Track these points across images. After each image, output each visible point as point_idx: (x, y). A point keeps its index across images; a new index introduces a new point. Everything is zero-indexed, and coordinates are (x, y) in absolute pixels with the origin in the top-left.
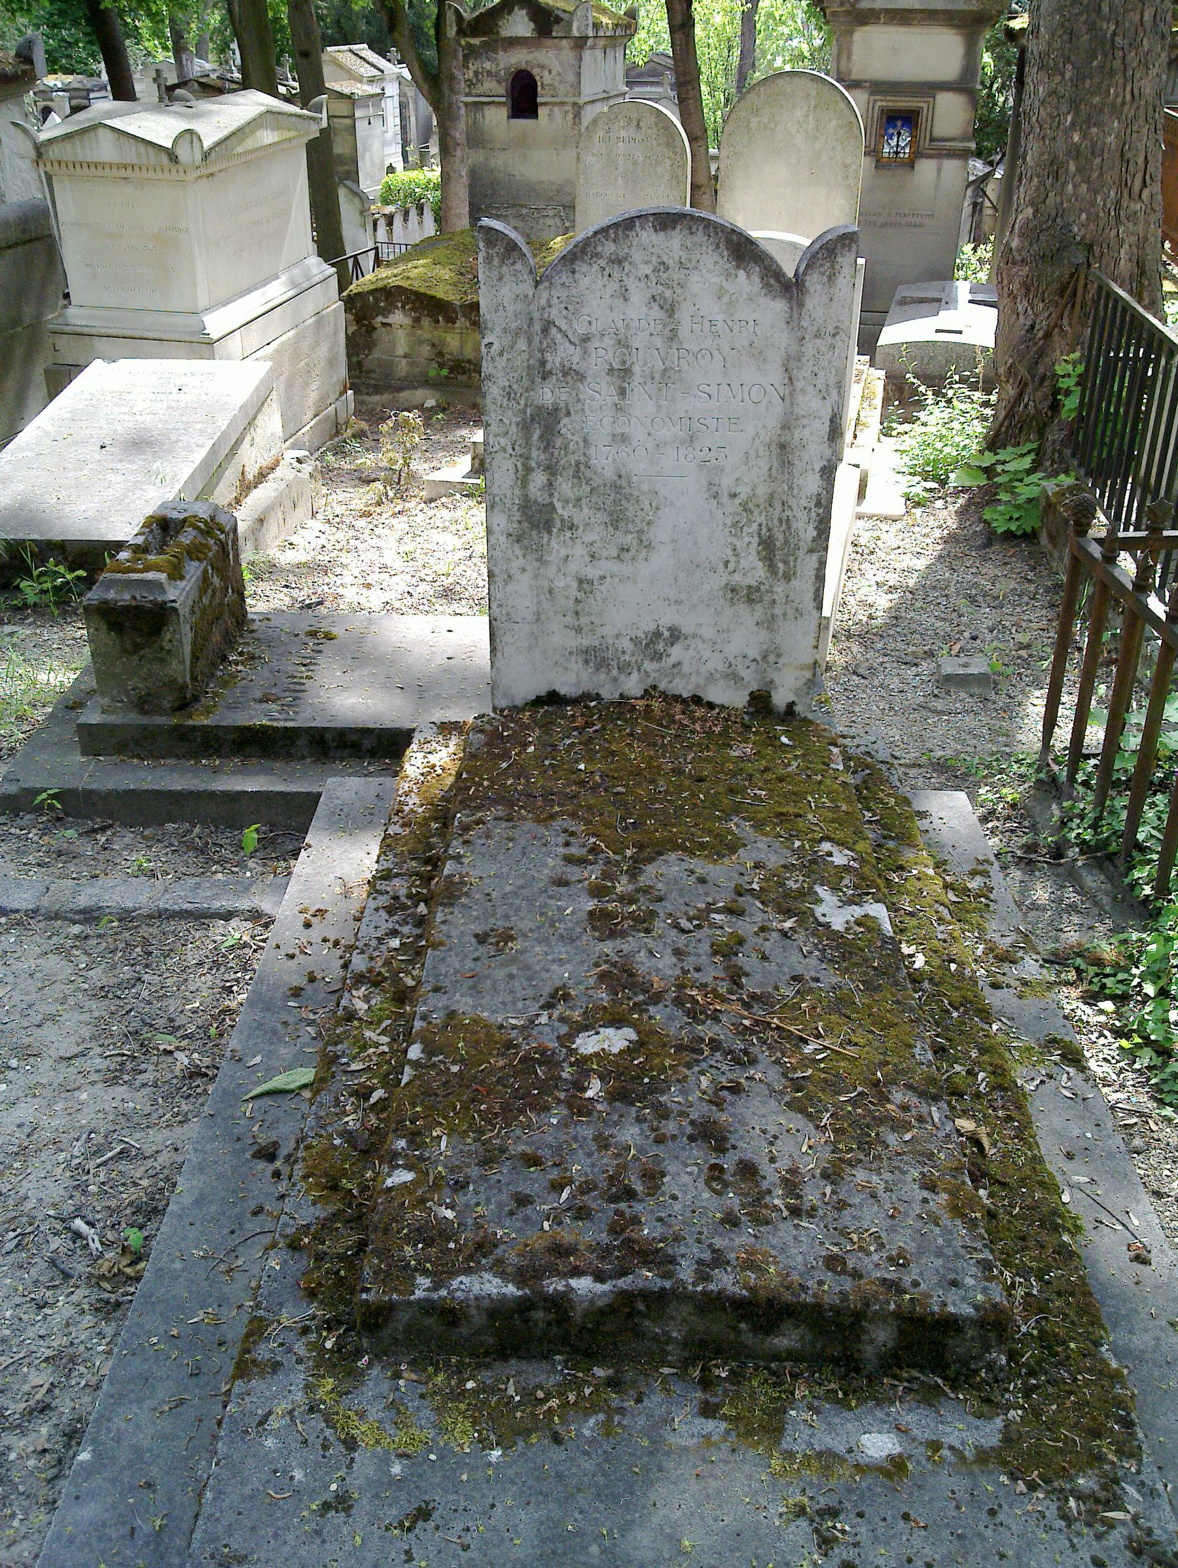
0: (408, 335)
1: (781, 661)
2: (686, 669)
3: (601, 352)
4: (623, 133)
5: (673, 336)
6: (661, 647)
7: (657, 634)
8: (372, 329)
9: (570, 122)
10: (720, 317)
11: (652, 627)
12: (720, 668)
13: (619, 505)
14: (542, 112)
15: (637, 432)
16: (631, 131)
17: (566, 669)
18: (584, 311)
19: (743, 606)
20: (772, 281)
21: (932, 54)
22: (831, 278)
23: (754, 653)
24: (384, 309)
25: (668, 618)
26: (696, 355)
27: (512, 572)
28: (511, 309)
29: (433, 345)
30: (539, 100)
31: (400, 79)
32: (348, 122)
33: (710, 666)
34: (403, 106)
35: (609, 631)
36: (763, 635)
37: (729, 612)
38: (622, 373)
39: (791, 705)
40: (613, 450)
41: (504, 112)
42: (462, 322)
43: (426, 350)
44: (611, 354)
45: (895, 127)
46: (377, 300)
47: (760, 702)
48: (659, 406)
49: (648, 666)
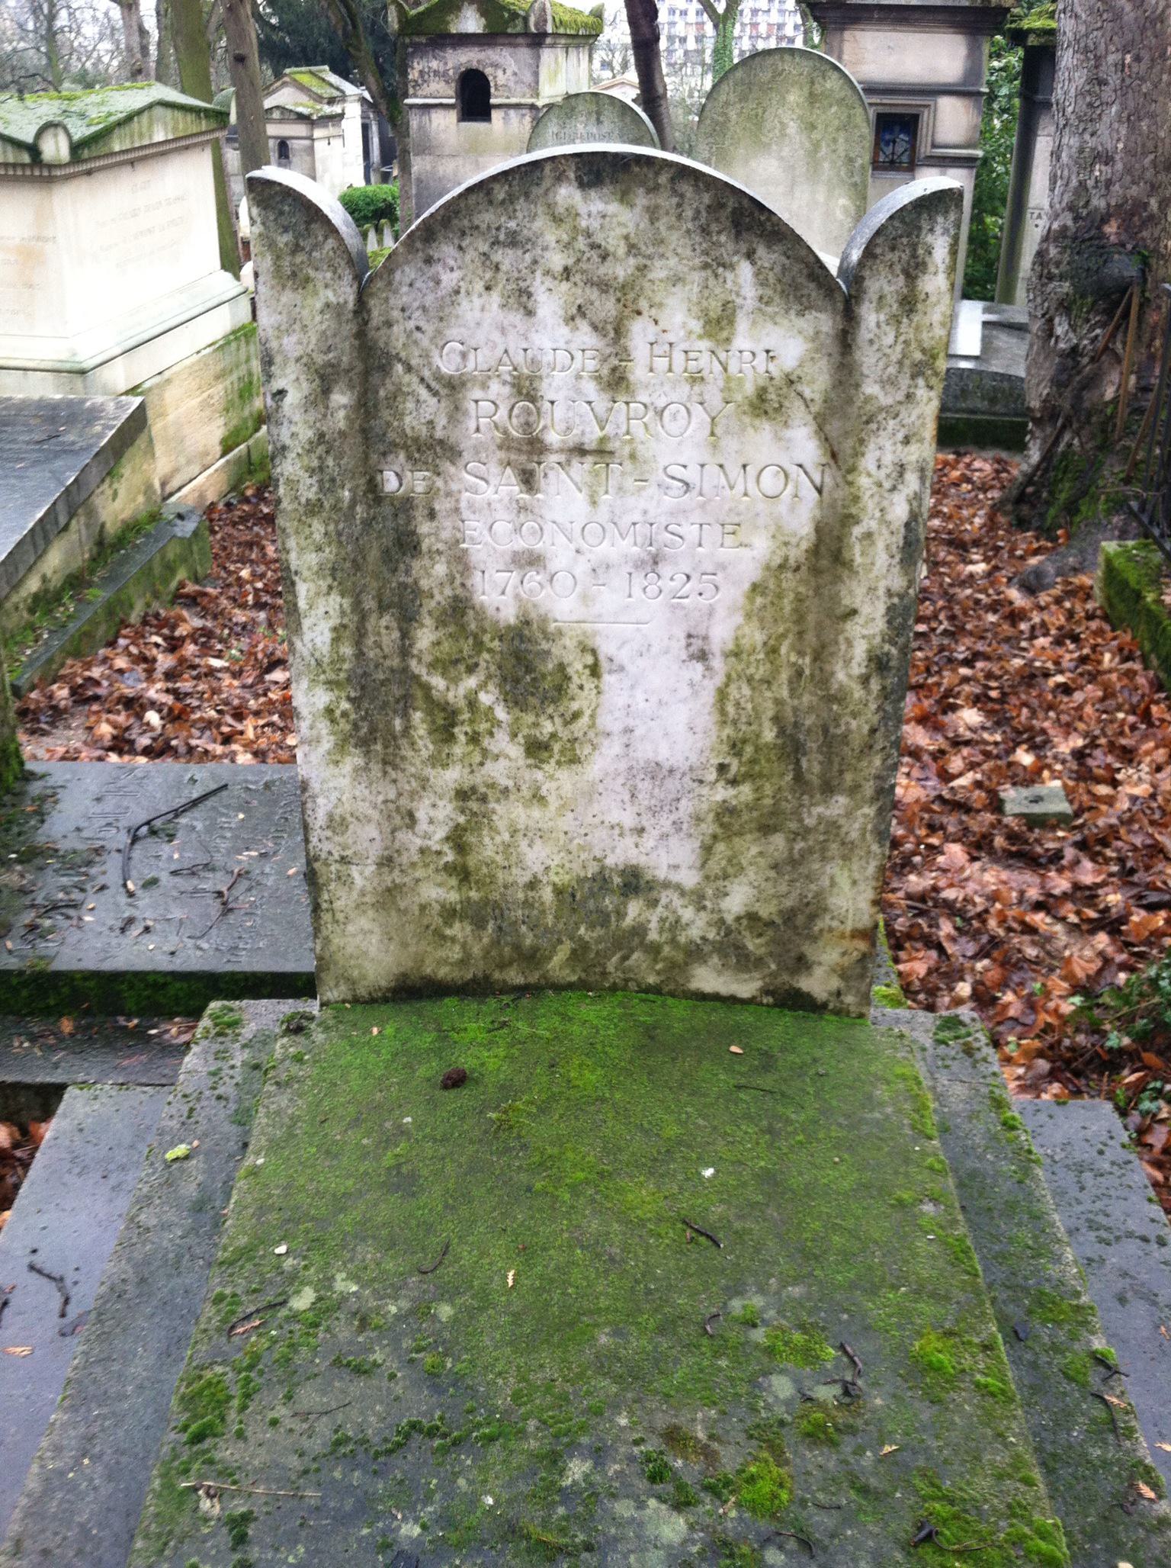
3: (486, 406)
13: (532, 670)
14: (496, 115)
15: (560, 554)
18: (453, 332)
21: (932, 57)
30: (493, 101)
31: (363, 100)
32: (307, 142)
33: (695, 933)
41: (453, 115)
44: (503, 412)
45: (892, 132)
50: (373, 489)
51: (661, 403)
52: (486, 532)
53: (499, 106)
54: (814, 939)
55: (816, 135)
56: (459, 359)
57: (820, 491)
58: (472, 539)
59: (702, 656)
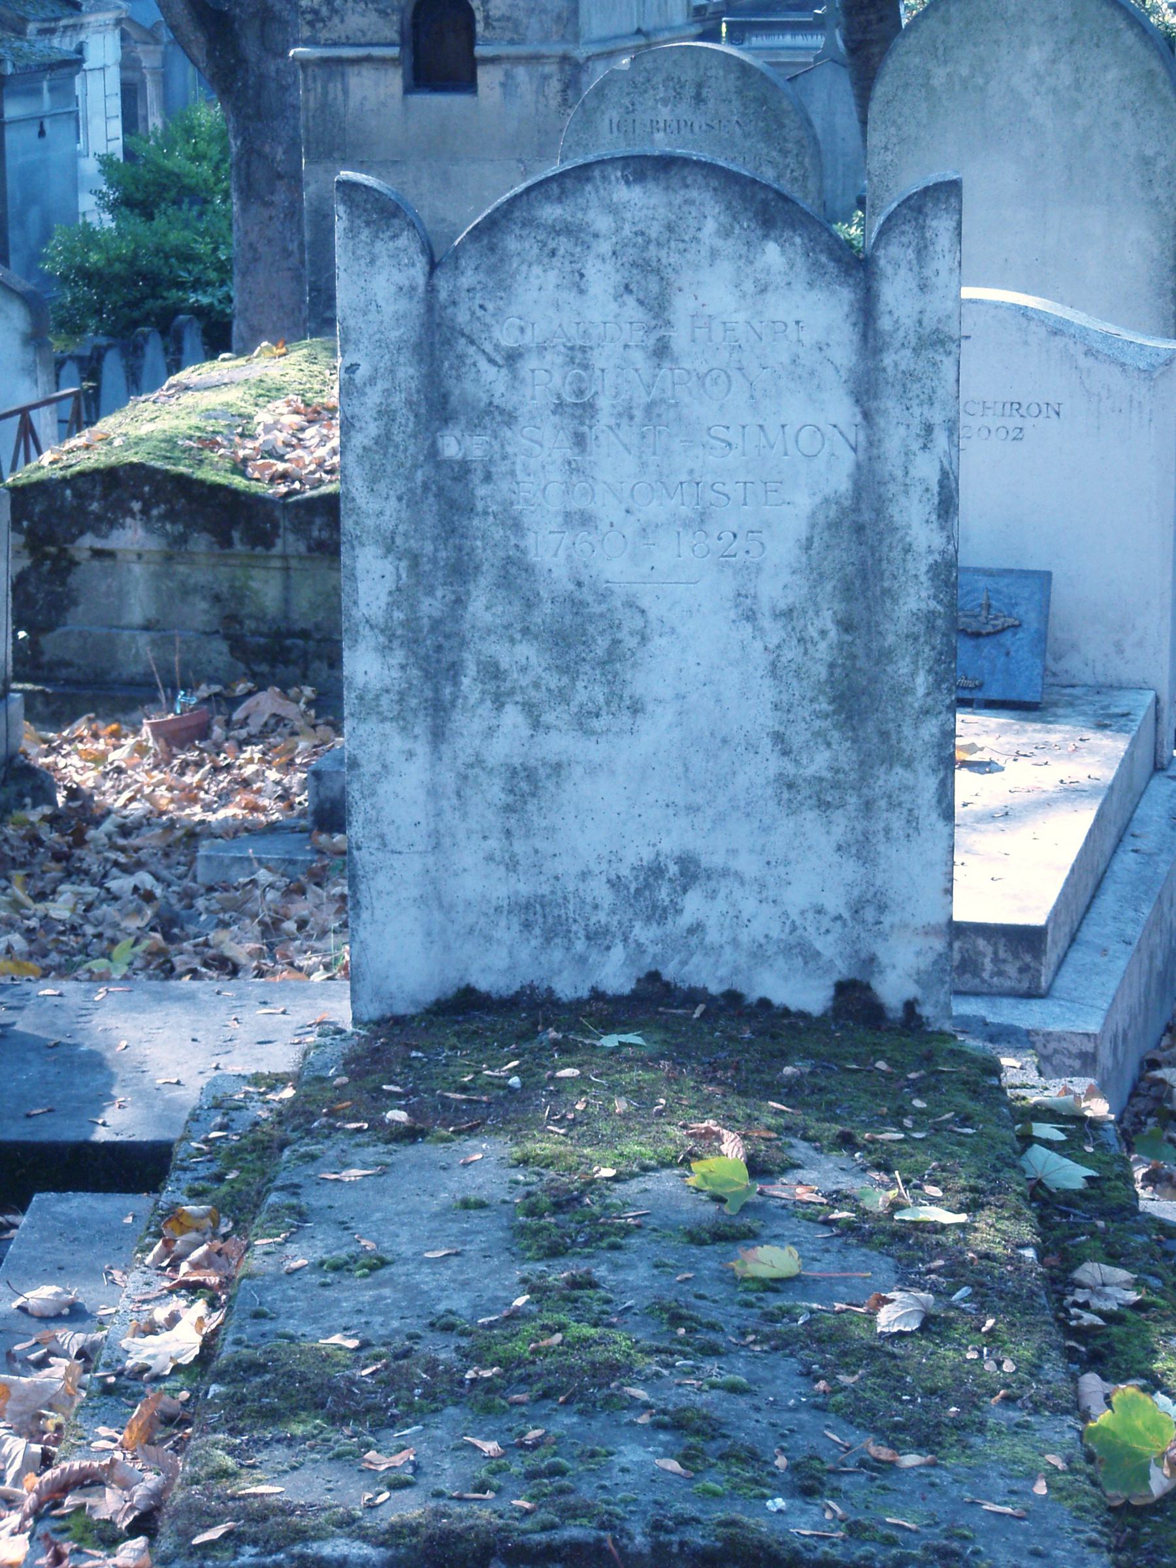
0: (156, 576)
1: (887, 919)
2: (713, 936)
3: (541, 375)
4: (665, 113)
5: (662, 351)
6: (663, 894)
7: (656, 871)
8: (65, 566)
9: (554, 102)
10: (741, 317)
11: (647, 855)
12: (775, 934)
14: (487, 77)
15: (607, 508)
16: (684, 110)
17: (489, 939)
18: (514, 309)
19: (811, 815)
20: (823, 259)
22: (922, 251)
23: (835, 903)
24: (99, 518)
25: (676, 839)
26: (701, 378)
27: (390, 758)
28: (389, 309)
29: (217, 599)
30: (480, 51)
33: (757, 929)
34: (130, 94)
35: (567, 866)
36: (851, 869)
37: (787, 826)
38: (578, 411)
39: (910, 1006)
40: (567, 538)
41: (394, 80)
42: (289, 543)
43: (200, 612)
46: (78, 495)
47: (854, 998)
48: (644, 465)
49: (643, 933)
50: (433, 453)
51: (703, 369)
52: (539, 494)
53: (494, 60)
54: (885, 937)
55: (1081, 120)
56: (517, 333)
57: (855, 450)
58: (526, 500)
59: (750, 616)
